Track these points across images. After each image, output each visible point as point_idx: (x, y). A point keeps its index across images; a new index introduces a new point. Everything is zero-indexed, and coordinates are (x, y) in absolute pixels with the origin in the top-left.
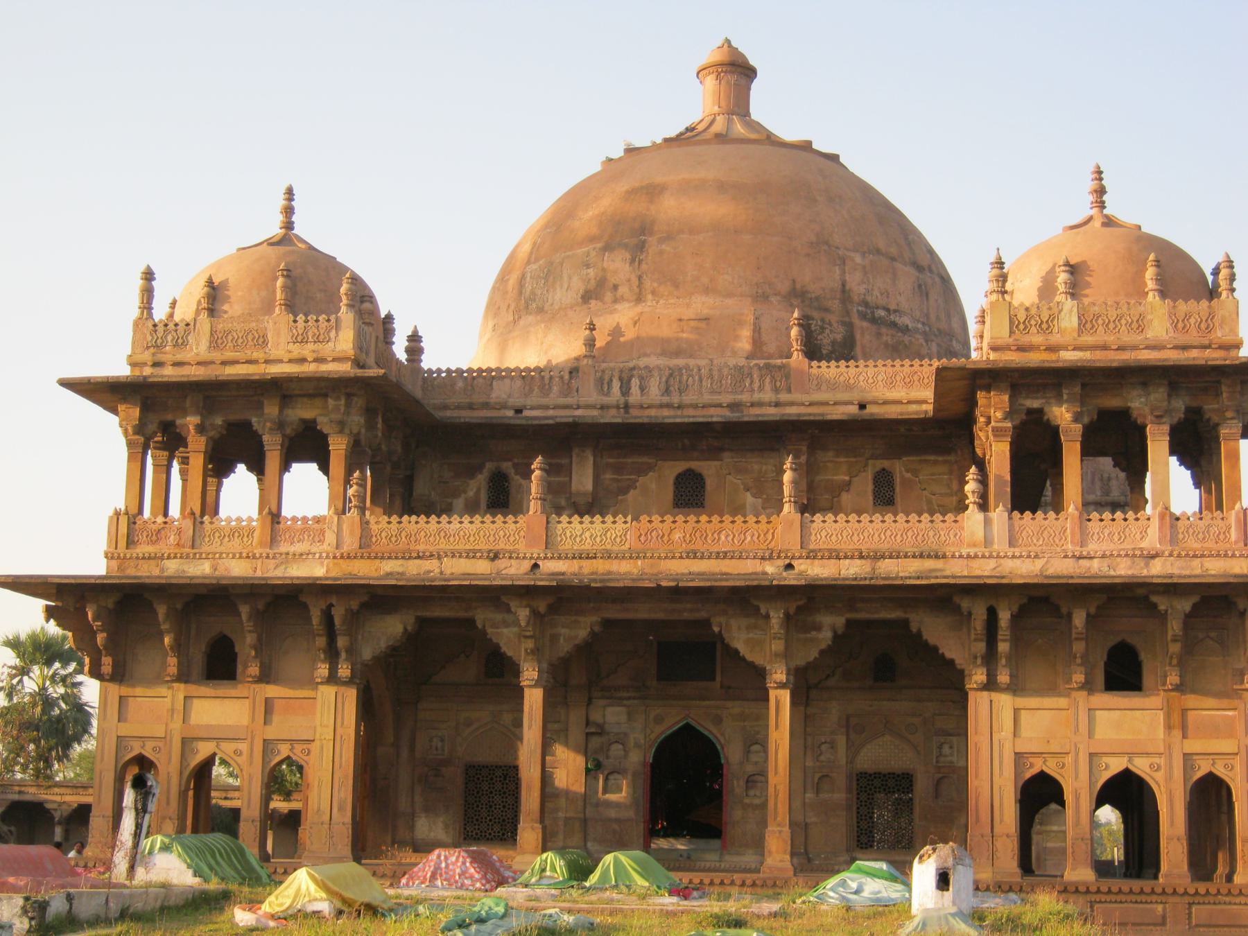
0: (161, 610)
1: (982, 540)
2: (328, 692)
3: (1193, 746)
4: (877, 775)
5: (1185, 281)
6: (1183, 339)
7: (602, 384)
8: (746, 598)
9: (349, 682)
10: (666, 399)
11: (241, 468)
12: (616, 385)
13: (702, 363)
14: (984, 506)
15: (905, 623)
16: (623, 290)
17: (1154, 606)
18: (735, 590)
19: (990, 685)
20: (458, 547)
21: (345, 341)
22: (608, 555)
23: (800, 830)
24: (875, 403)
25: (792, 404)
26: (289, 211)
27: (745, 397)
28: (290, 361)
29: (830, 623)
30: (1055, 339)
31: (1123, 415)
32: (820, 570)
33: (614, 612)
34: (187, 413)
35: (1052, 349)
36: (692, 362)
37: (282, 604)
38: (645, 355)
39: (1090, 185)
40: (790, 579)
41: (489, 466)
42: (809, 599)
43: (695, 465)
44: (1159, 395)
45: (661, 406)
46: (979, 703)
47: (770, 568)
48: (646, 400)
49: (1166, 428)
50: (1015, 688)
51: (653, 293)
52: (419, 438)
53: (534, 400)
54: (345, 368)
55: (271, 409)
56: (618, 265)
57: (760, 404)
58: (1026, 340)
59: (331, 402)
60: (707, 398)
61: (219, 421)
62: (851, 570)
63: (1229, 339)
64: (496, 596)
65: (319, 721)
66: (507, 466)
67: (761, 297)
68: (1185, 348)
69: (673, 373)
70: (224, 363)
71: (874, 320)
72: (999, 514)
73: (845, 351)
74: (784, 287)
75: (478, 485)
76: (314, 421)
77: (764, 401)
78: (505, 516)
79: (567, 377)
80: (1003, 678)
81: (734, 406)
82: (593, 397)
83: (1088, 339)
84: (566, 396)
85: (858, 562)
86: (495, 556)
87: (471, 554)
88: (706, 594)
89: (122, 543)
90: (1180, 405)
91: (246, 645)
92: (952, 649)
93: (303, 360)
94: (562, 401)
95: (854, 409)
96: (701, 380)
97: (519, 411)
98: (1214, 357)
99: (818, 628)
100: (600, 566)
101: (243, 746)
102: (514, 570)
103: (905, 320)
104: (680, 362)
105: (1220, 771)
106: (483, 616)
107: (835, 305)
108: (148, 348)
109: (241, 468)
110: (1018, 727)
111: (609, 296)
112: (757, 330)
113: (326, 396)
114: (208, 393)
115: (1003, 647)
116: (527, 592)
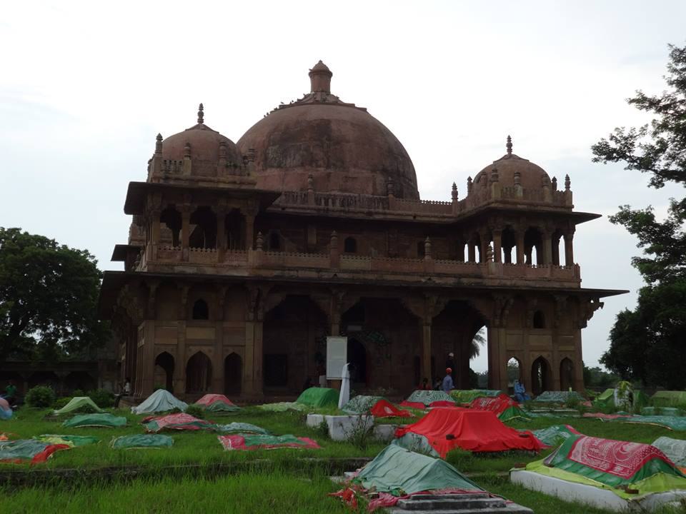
2: (250, 327)
3: (562, 348)
7: (318, 201)
8: (420, 292)
10: (343, 208)
12: (323, 201)
13: (356, 195)
14: (255, 248)
16: (321, 162)
22: (364, 272)
24: (420, 216)
26: (201, 114)
27: (372, 210)
28: (229, 183)
30: (515, 200)
35: (516, 203)
36: (352, 194)
37: (237, 286)
38: (333, 190)
42: (350, 287)
45: (341, 211)
47: (423, 280)
48: (336, 208)
51: (334, 165)
53: (290, 205)
59: (249, 202)
60: (358, 209)
61: (196, 206)
65: (250, 343)
68: (556, 207)
70: (199, 181)
84: (303, 204)
85: (453, 279)
86: (319, 270)
87: (310, 269)
93: (235, 183)
94: (301, 206)
95: (411, 218)
97: (283, 209)
100: (361, 276)
102: (326, 275)
104: (347, 194)
108: (162, 171)
111: (314, 165)
112: (374, 184)
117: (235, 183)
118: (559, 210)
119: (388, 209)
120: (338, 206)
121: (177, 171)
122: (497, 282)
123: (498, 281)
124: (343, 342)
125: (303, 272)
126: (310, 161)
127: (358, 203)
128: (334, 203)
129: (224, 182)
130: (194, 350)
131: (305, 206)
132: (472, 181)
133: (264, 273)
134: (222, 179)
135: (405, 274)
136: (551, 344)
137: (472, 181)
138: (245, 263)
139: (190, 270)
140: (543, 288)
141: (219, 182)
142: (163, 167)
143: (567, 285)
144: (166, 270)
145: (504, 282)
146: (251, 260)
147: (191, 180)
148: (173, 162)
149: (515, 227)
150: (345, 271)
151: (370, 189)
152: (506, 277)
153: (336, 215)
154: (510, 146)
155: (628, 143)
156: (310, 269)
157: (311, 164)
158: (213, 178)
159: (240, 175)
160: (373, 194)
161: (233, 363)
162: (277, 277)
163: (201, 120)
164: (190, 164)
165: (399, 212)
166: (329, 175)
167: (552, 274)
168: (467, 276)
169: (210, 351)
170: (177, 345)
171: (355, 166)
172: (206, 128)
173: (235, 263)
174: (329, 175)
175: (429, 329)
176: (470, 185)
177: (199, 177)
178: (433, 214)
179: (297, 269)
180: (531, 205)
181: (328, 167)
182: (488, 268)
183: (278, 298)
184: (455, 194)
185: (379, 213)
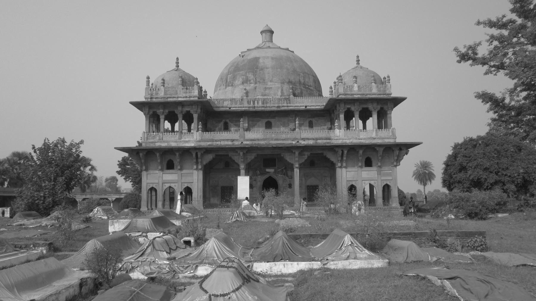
0: (158, 154)
1: (339, 135)
2: (195, 172)
3: (383, 178)
4: (311, 186)
5: (383, 82)
6: (379, 93)
7: (249, 102)
8: (290, 149)
9: (201, 169)
15: (322, 154)
16: (252, 81)
17: (376, 149)
18: (288, 147)
19: (341, 167)
20: (223, 138)
21: (196, 93)
22: (258, 140)
25: (291, 106)
26: (177, 63)
27: (280, 105)
29: (307, 154)
30: (353, 93)
31: (367, 109)
32: (303, 143)
33: (260, 153)
34: (156, 111)
35: (352, 95)
37: (185, 152)
39: (356, 59)
40: (298, 144)
41: (224, 120)
43: (269, 120)
44: (375, 105)
46: (338, 170)
47: (294, 143)
48: (259, 106)
49: (376, 112)
50: (346, 167)
51: (259, 82)
52: (210, 115)
53: (233, 106)
54: (196, 99)
55: (180, 108)
56: (251, 76)
57: (284, 106)
58: (347, 93)
60: (272, 105)
61: (167, 111)
62: (311, 142)
63: (389, 93)
64: (234, 149)
65: (195, 178)
66: (228, 121)
67: (283, 83)
70: (168, 98)
72: (342, 131)
73: (301, 95)
74: (287, 81)
75: (221, 125)
76: (189, 111)
77: (285, 106)
80: (344, 165)
81: (278, 107)
82: (246, 105)
83: (360, 93)
86: (233, 140)
87: (228, 140)
89: (146, 139)
90: (379, 107)
91: (176, 162)
92: (333, 159)
94: (240, 106)
95: (304, 107)
98: (385, 96)
99: (304, 155)
100: (257, 142)
101: (176, 184)
102: (237, 144)
104: (266, 97)
105: (388, 183)
106: (231, 154)
110: (347, 175)
111: (248, 83)
112: (282, 90)
113: (192, 105)
114: (165, 105)
115: (345, 158)
116: (242, 149)
117: (187, 97)
118: (382, 96)
120: (260, 104)
121: (157, 94)
122: (339, 142)
123: (341, 141)
124: (247, 179)
126: (246, 81)
127: (272, 102)
131: (242, 106)
135: (282, 140)
136: (376, 176)
138: (193, 138)
139: (164, 145)
145: (344, 141)
146: (195, 137)
149: (353, 109)
150: (247, 140)
151: (279, 93)
152: (346, 138)
153: (260, 109)
155: (473, 48)
156: (228, 140)
157: (247, 83)
161: (188, 191)
164: (163, 90)
166: (255, 88)
167: (376, 135)
169: (175, 186)
171: (271, 81)
173: (187, 139)
177: (168, 96)
178: (317, 104)
179: (220, 140)
180: (363, 94)
181: (256, 83)
183: (209, 157)
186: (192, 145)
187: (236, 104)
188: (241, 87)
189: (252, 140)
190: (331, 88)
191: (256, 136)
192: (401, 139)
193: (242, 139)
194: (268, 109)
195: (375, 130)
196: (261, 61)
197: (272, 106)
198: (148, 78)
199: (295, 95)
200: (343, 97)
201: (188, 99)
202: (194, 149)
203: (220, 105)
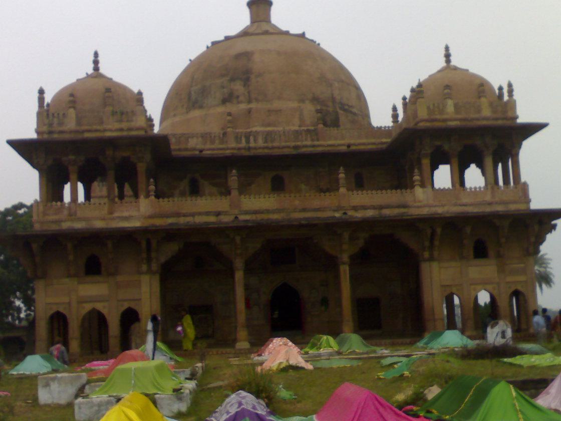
0: (70, 246)
2: (145, 279)
3: (509, 279)
7: (238, 139)
8: (332, 228)
10: (266, 145)
11: (473, 166)
12: (244, 140)
16: (241, 98)
22: (268, 211)
23: (249, 326)
24: (355, 145)
25: (319, 146)
26: (96, 62)
27: (299, 143)
30: (445, 117)
32: (359, 215)
35: (445, 120)
36: (275, 129)
42: (355, 226)
45: (264, 148)
46: (425, 267)
47: (337, 215)
53: (208, 146)
57: (306, 146)
58: (434, 117)
60: (283, 144)
62: (370, 213)
64: (221, 231)
68: (497, 119)
69: (269, 134)
70: (83, 132)
71: (345, 110)
75: (184, 185)
78: (401, 190)
79: (221, 136)
80: (436, 253)
81: (296, 147)
82: (233, 144)
83: (459, 116)
86: (218, 214)
87: (208, 214)
88: (311, 226)
94: (221, 146)
96: (280, 136)
97: (201, 151)
100: (265, 216)
102: (226, 219)
103: (354, 110)
107: (330, 104)
109: (473, 166)
114: (77, 145)
115: (437, 243)
119: (318, 140)
121: (61, 124)
122: (425, 211)
125: (200, 217)
128: (255, 141)
129: (111, 130)
130: (88, 307)
132: (407, 100)
133: (159, 222)
134: (109, 127)
135: (318, 210)
137: (407, 100)
138: (138, 212)
139: (79, 225)
140: (482, 212)
141: (105, 130)
142: (46, 121)
143: (513, 207)
144: (54, 227)
145: (433, 210)
147: (77, 132)
148: (56, 115)
149: (446, 147)
150: (246, 213)
151: (297, 121)
154: (448, 56)
156: (208, 214)
158: (98, 127)
159: (128, 121)
160: (300, 126)
162: (171, 224)
163: (96, 69)
164: (74, 116)
165: (330, 142)
168: (388, 207)
169: (104, 307)
170: (69, 303)
172: (456, 68)
173: (126, 214)
174: (249, 111)
175: (347, 268)
176: (405, 105)
181: (250, 102)
182: (414, 195)
183: (171, 249)
184: (395, 116)
185: (307, 145)
186: (137, 224)
187: (213, 142)
188: (221, 109)
189: (256, 212)
190: (395, 109)
191: (260, 204)
192: (538, 202)
193: (236, 211)
194: (277, 152)
195: (489, 187)
196: (257, 58)
197: (283, 145)
198: (41, 92)
199: (325, 124)
200: (428, 124)
201: (125, 133)
202: (144, 231)
203: (183, 146)
